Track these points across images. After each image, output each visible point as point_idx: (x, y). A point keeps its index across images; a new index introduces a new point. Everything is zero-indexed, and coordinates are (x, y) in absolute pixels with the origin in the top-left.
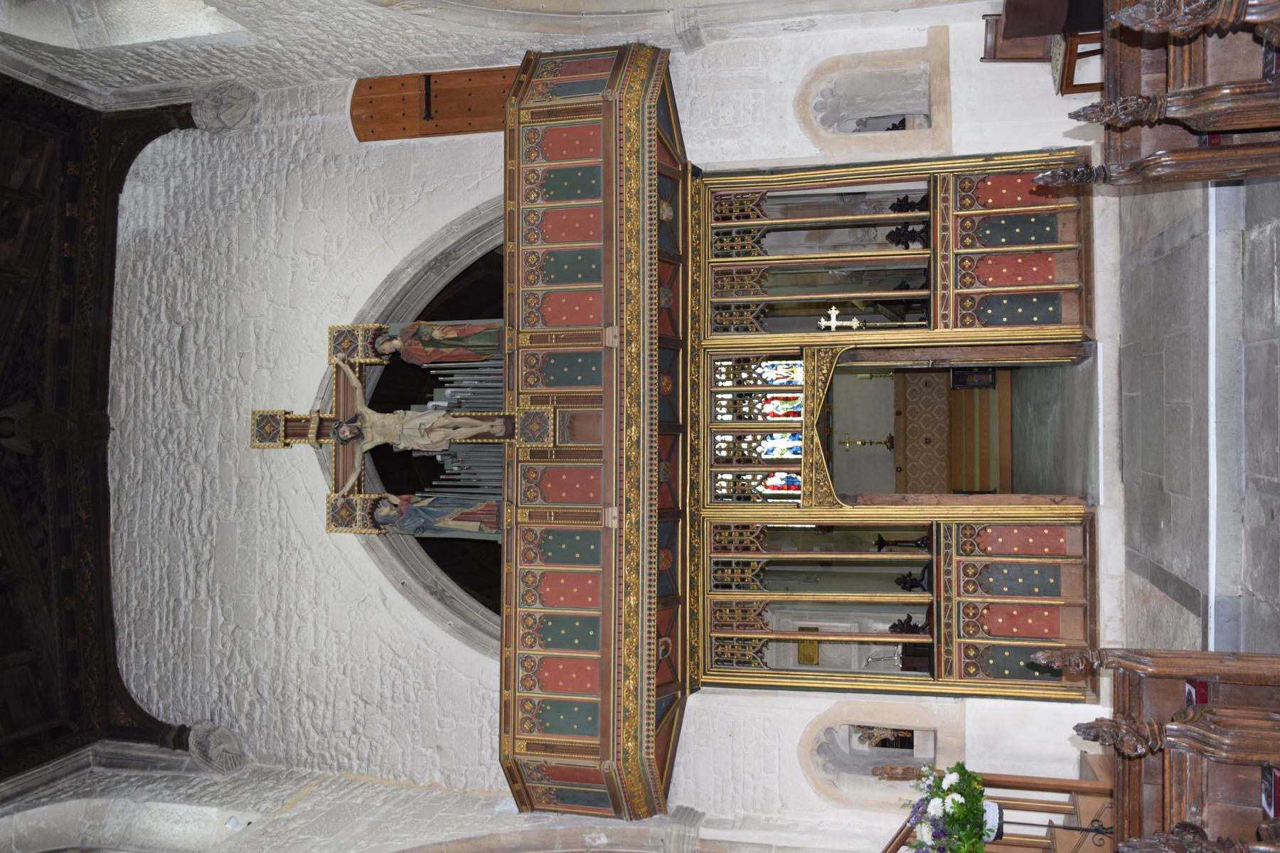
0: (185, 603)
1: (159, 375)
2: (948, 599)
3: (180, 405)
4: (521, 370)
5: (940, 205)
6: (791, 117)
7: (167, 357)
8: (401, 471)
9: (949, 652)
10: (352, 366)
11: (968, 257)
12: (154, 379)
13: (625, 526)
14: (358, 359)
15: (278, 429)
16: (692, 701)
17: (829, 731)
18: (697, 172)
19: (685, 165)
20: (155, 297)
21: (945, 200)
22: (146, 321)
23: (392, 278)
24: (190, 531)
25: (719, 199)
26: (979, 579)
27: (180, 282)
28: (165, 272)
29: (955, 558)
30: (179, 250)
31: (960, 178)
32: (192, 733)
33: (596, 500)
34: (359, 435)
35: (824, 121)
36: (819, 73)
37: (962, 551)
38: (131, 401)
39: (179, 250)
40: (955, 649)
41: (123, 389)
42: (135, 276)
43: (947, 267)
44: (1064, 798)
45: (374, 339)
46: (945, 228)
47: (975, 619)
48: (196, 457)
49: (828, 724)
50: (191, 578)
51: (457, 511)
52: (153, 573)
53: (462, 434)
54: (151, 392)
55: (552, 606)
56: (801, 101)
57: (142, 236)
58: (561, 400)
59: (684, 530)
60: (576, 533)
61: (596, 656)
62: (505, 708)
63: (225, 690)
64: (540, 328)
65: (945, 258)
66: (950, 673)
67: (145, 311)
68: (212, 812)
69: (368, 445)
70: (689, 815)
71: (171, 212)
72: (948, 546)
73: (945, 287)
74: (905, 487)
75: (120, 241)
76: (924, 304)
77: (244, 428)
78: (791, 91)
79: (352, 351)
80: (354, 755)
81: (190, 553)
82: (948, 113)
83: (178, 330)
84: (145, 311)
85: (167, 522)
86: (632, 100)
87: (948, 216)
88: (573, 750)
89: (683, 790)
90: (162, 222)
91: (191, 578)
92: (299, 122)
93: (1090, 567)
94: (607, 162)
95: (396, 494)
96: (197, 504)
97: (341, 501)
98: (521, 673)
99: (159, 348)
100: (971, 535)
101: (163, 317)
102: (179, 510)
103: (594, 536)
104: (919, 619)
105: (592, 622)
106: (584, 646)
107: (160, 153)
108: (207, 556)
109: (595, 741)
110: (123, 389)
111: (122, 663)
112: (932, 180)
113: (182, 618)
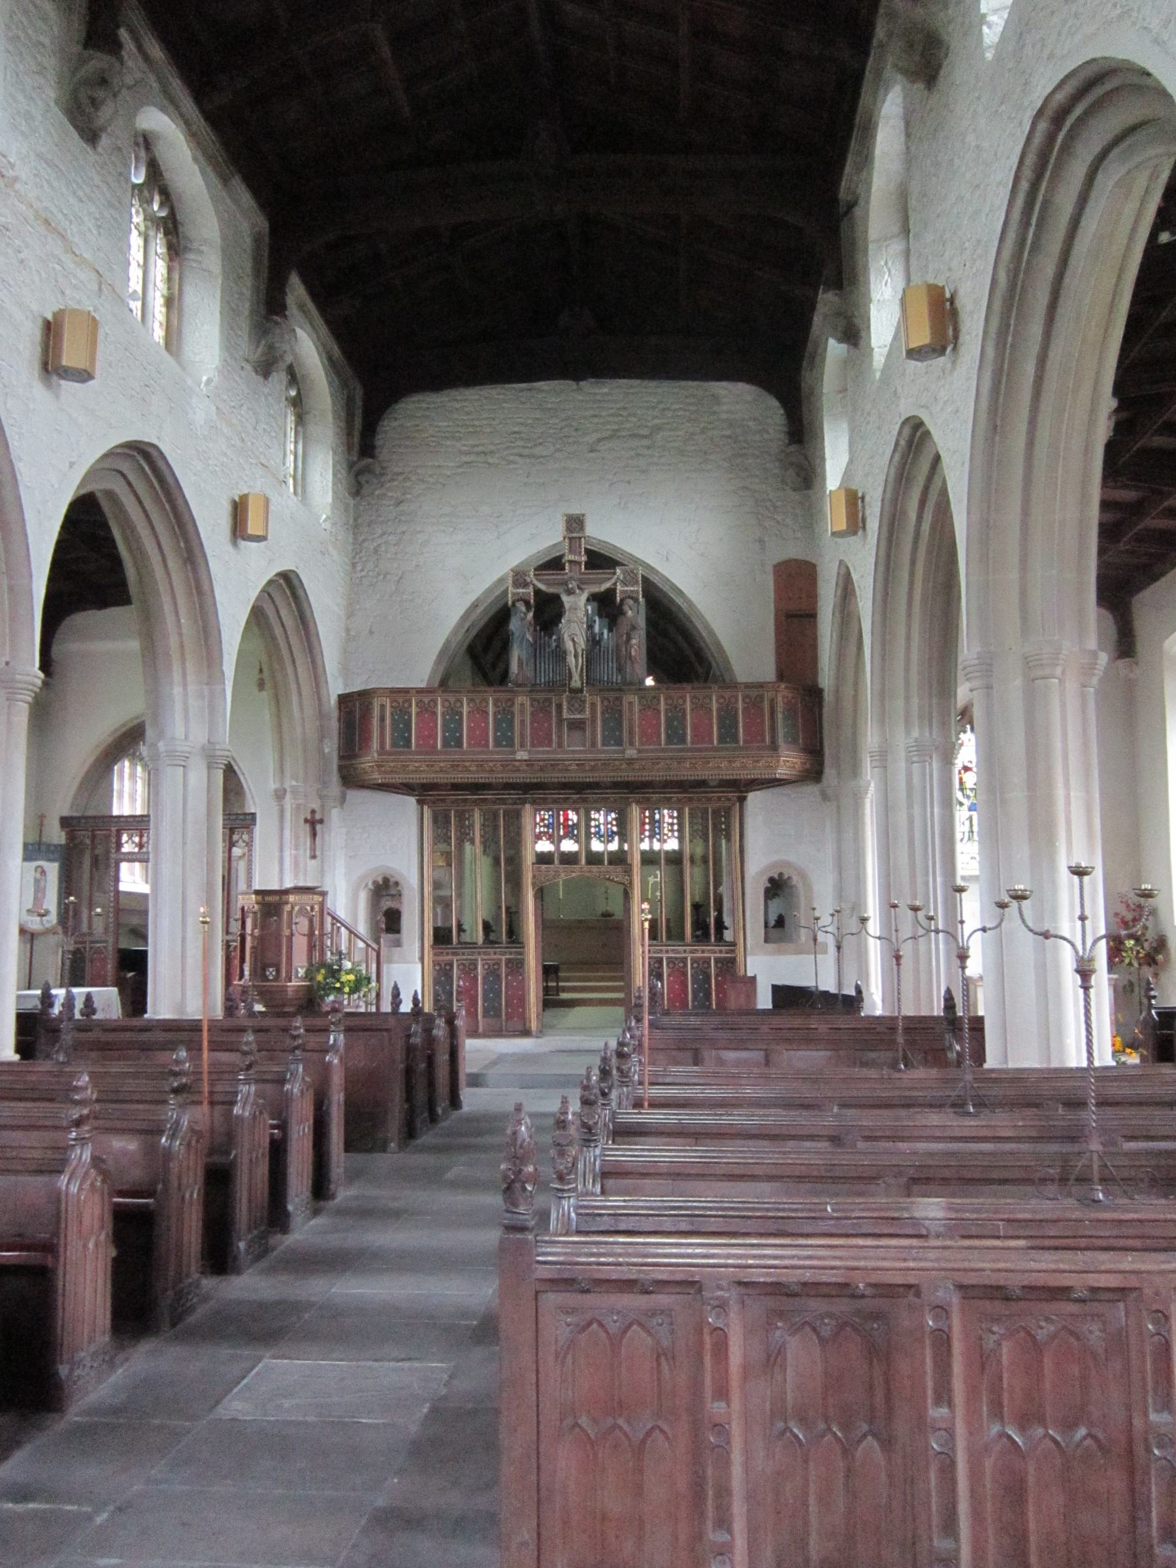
0: (458, 445)
1: (616, 419)
2: (479, 953)
3: (595, 436)
4: (727, 694)
5: (717, 948)
6: (776, 858)
7: (628, 425)
8: (548, 611)
9: (447, 954)
10: (615, 584)
11: (685, 966)
12: (613, 415)
13: (517, 764)
14: (619, 587)
15: (575, 523)
16: (412, 800)
17: (397, 884)
18: (742, 800)
19: (747, 792)
20: (670, 414)
21: (721, 952)
22: (653, 408)
23: (680, 593)
24: (508, 448)
25: (728, 811)
26: (493, 973)
27: (680, 433)
28: (688, 421)
29: (503, 958)
30: (703, 431)
31: (733, 961)
32: (370, 460)
33: (533, 745)
34: (570, 592)
35: (771, 880)
36: (803, 876)
37: (509, 961)
38: (598, 397)
39: (703, 431)
40: (450, 957)
41: (606, 390)
42: (687, 397)
43: (679, 953)
44: (564, 996)
45: (632, 598)
46: (703, 952)
47: (469, 970)
48: (557, 450)
49: (402, 882)
50: (476, 449)
51: (524, 658)
52: (478, 419)
53: (571, 660)
54: (604, 414)
55: (468, 718)
56: (788, 864)
57: (716, 399)
58: (594, 720)
59: (514, 795)
60: (513, 733)
61: (439, 746)
62: (406, 691)
63: (401, 478)
64: (636, 708)
65: (685, 951)
66: (435, 954)
67: (661, 406)
68: (329, 499)
69: (565, 598)
70: (343, 799)
71: (731, 424)
72: (511, 953)
73: (667, 952)
74: (546, 926)
75: (713, 383)
76: (676, 934)
77: (575, 510)
78: (791, 858)
79: (624, 584)
80: (363, 574)
81: (492, 447)
82: (772, 953)
83: (645, 432)
84: (661, 406)
85: (516, 429)
86: (788, 761)
87: (712, 953)
88: (380, 734)
89: (354, 795)
90: (725, 416)
91: (476, 449)
92: (789, 521)
93: (967, 563)
94: (741, 749)
95: (534, 617)
96: (526, 452)
97: (529, 580)
98: (426, 700)
99: (634, 419)
100: (517, 966)
101: (657, 421)
102: (522, 439)
103: (511, 743)
104: (466, 937)
105: (459, 743)
106: (444, 738)
107: (772, 411)
108: (491, 461)
109: (388, 747)
110: (606, 390)
111: (416, 398)
112: (733, 944)
113: (449, 443)
